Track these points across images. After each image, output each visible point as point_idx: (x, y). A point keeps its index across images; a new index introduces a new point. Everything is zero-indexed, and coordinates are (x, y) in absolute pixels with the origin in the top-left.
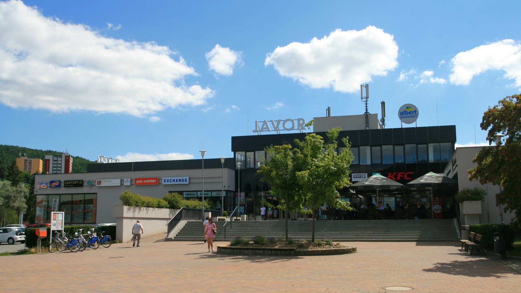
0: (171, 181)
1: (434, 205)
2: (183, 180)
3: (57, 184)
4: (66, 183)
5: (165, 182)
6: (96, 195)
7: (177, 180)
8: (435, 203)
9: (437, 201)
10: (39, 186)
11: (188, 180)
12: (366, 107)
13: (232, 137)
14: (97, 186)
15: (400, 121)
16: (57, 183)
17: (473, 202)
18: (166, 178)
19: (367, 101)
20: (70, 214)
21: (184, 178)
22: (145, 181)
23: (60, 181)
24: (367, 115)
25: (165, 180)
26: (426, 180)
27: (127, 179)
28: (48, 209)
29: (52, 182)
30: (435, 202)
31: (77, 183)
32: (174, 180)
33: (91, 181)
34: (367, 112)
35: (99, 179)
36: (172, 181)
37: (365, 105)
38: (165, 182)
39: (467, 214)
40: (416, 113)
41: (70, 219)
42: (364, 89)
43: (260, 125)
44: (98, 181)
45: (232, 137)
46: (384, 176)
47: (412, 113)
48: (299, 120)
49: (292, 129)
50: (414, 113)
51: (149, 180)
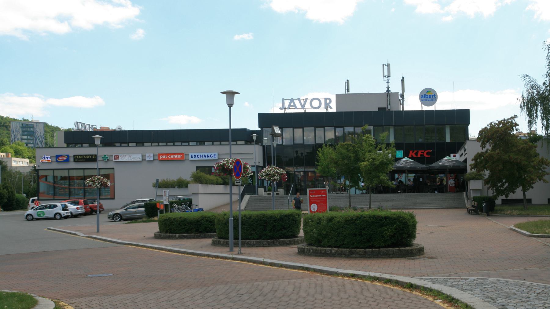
0: (198, 156)
1: (450, 179)
2: (212, 156)
3: (65, 158)
4: (76, 157)
5: (191, 157)
6: (112, 170)
7: (205, 155)
8: (450, 177)
9: (452, 176)
10: (42, 160)
11: (217, 156)
12: (388, 85)
13: (259, 114)
14: (114, 160)
15: (421, 103)
16: (65, 157)
17: (476, 180)
18: (193, 154)
19: (388, 80)
20: (83, 190)
21: (213, 154)
22: (170, 157)
23: (68, 156)
24: (388, 94)
25: (191, 155)
26: (444, 163)
27: (150, 154)
28: (55, 185)
29: (57, 156)
30: (450, 176)
31: (89, 157)
32: (201, 156)
33: (107, 156)
34: (388, 91)
35: (116, 154)
36: (200, 156)
37: (387, 84)
38: (191, 157)
39: (472, 189)
40: (435, 97)
41: (83, 194)
42: (386, 68)
43: (287, 103)
44: (115, 156)
45: (259, 114)
46: (412, 159)
47: (431, 97)
48: (326, 99)
49: (319, 107)
50: (433, 96)
51: (174, 156)
